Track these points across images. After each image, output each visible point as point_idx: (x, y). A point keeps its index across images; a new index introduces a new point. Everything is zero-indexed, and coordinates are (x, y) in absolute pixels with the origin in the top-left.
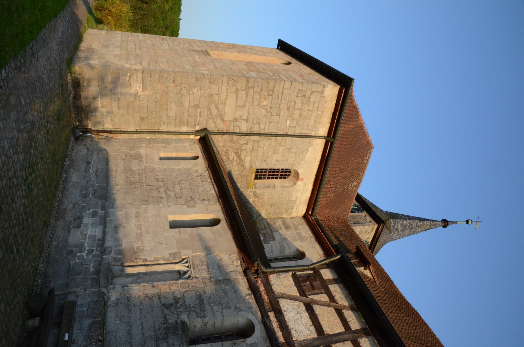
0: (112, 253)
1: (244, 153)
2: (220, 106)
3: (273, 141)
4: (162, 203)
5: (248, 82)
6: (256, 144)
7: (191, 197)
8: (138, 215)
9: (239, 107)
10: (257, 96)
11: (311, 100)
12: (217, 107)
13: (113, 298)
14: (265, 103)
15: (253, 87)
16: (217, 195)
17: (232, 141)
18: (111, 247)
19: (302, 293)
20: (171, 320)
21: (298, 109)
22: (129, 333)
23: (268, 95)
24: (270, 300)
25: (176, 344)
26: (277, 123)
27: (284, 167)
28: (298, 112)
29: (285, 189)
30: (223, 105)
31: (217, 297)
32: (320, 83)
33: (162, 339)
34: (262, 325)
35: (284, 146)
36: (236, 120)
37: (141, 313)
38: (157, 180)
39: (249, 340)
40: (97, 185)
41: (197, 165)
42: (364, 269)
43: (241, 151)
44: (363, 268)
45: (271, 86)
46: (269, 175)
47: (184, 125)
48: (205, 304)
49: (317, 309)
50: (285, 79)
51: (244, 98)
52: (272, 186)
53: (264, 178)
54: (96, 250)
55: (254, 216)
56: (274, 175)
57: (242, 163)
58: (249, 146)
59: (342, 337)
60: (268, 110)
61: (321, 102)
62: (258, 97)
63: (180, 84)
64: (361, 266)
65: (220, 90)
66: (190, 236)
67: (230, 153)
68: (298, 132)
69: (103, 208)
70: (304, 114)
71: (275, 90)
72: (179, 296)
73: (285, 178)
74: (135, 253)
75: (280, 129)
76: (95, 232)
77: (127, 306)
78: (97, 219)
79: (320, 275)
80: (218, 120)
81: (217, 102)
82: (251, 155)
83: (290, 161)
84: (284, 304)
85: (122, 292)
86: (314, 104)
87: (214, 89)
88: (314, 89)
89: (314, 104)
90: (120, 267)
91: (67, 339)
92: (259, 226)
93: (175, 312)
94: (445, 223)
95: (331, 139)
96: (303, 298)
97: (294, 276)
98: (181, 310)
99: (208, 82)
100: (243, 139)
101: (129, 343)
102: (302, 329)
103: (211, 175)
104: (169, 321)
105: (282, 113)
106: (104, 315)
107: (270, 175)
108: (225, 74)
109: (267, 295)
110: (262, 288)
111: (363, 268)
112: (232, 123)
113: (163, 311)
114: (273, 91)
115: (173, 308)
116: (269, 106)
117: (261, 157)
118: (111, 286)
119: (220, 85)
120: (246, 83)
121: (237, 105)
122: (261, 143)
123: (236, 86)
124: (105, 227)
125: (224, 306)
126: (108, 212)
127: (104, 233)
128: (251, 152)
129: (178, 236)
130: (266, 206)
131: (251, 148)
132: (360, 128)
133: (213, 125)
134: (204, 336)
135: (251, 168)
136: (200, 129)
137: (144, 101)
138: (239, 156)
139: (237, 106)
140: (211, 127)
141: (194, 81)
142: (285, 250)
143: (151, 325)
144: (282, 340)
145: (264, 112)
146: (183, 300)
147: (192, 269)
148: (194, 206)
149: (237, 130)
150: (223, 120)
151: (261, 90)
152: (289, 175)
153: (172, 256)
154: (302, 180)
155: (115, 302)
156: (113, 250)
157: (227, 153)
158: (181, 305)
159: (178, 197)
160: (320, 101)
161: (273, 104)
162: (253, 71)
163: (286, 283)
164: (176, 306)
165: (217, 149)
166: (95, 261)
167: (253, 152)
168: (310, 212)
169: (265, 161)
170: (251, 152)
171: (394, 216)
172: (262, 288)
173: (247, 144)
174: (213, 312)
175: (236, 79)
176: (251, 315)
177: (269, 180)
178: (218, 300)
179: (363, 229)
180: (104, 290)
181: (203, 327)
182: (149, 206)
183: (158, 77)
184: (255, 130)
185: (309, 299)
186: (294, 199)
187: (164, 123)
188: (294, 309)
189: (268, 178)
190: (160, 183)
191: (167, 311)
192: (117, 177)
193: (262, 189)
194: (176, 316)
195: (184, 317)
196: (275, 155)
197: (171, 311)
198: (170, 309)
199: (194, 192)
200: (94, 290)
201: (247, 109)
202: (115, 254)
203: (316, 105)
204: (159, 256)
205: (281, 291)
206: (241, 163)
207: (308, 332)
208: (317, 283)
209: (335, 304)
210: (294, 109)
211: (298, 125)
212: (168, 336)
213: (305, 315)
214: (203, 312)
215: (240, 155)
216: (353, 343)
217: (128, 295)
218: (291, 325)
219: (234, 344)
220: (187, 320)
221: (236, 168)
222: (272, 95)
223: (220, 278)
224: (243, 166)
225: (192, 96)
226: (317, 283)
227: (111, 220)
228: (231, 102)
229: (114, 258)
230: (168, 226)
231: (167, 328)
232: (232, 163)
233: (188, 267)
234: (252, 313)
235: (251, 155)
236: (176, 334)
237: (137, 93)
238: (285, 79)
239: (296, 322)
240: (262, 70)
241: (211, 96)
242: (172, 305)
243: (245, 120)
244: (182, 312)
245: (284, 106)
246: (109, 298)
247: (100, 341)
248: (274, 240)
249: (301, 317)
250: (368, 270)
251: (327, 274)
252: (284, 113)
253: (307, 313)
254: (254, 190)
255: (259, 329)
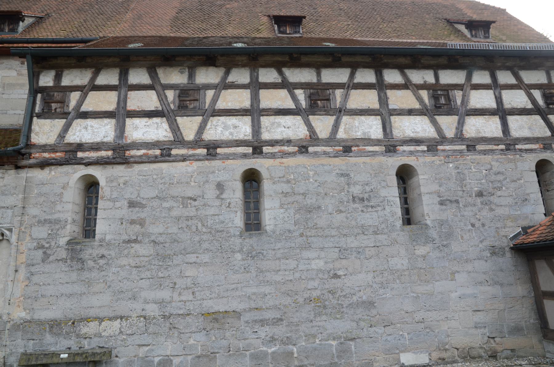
13: (23, 314)
19: (65, 115)
20: (63, 254)
24: (63, 151)
33: (83, 265)
34: (89, 167)
37: (49, 284)
39: (102, 182)
42: (23, 21)
44: (21, 23)
48: (51, 218)
59: (122, 96)
64: (18, 23)
91: (67, 355)
93: (54, 250)
96: (70, 117)
98: (53, 244)
101: (81, 296)
104: (64, 256)
106: (40, 323)
109: (57, 152)
110: (46, 155)
111: (21, 23)
115: (49, 252)
125: (58, 199)
134: (84, 224)
144: (110, 153)
155: (28, 311)
158: (48, 243)
164: (47, 248)
172: (46, 155)
174: (63, 212)
178: (49, 204)
188: (80, 131)
191: (51, 258)
194: (60, 249)
195: (63, 241)
198: (50, 255)
205: (56, 137)
207: (109, 126)
208: (57, 96)
209: (86, 88)
212: (81, 259)
213: (90, 122)
214: (60, 221)
216: (131, 90)
217: (22, 299)
219: (102, 198)
220: (67, 239)
223: (21, 196)
226: (57, 96)
234: (74, 173)
236: (81, 251)
239: (96, 133)
244: (56, 243)
249: (92, 126)
251: (47, 80)
253: (89, 120)
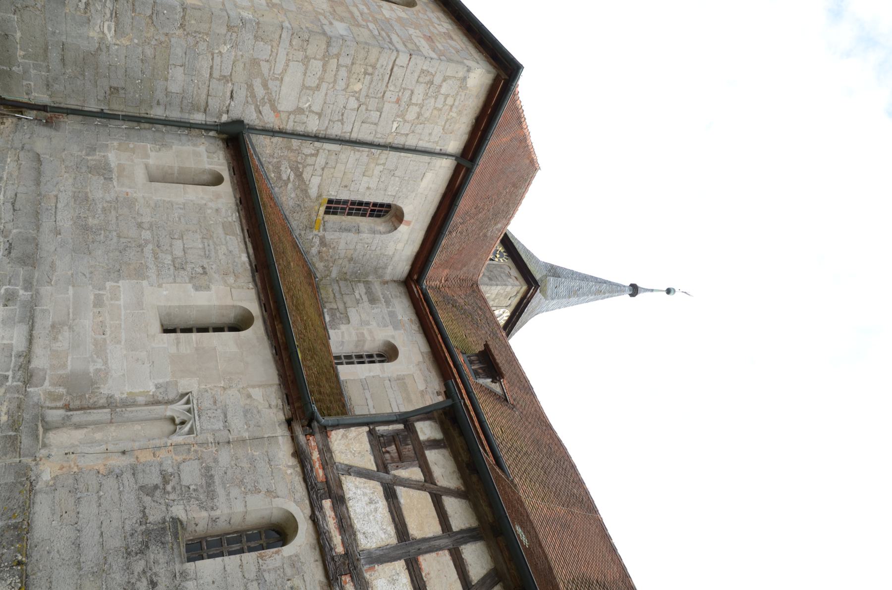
0: (47, 383)
1: (309, 169)
2: (271, 84)
3: (365, 154)
4: (148, 277)
5: (329, 44)
6: (333, 157)
7: (203, 268)
8: (99, 302)
9: (308, 88)
10: (343, 73)
11: (443, 90)
12: (265, 85)
13: (46, 477)
14: (357, 87)
15: (338, 56)
16: (251, 265)
17: (289, 148)
18: (43, 369)
20: (155, 516)
21: (416, 105)
22: (77, 545)
23: (366, 73)
25: (161, 561)
26: (375, 124)
27: (379, 200)
28: (417, 109)
29: (378, 236)
30: (278, 82)
31: (238, 471)
32: (462, 63)
33: (137, 554)
34: (310, 522)
35: (384, 164)
36: (299, 111)
38: (140, 225)
39: (288, 550)
40: (15, 231)
41: (218, 196)
42: (492, 382)
43: (304, 167)
45: (372, 59)
46: (350, 209)
47: (198, 110)
48: (217, 484)
49: (401, 491)
50: (400, 47)
51: (319, 73)
52: (353, 230)
53: (342, 213)
54: (14, 378)
55: (318, 275)
56: (359, 210)
57: (304, 187)
58: (321, 160)
59: (437, 543)
60: (362, 100)
61: (459, 97)
62: (346, 74)
63: (195, 32)
64: (488, 377)
65: (274, 54)
66: (197, 349)
67: (283, 168)
68: (411, 142)
69: (28, 285)
70: (427, 114)
71: (378, 66)
72: (170, 470)
73: (378, 216)
74: (93, 383)
75: (379, 136)
76: (11, 338)
77: (73, 491)
78: (16, 308)
79: (414, 432)
80: (266, 109)
81: (266, 75)
82: (321, 176)
83: (391, 191)
84: (352, 487)
85: (65, 464)
86: (446, 99)
87: (263, 51)
88: (449, 73)
89: (446, 99)
90: (62, 412)
92: (323, 296)
93: (162, 501)
94: (634, 290)
95: (466, 164)
96: (382, 475)
97: (371, 433)
98: (172, 497)
99: (252, 37)
100: (308, 148)
101: (76, 564)
102: (375, 531)
103: (244, 221)
104: (151, 519)
105: (387, 107)
106: (27, 508)
107: (352, 209)
108: (286, 24)
109: (324, 469)
110: (316, 455)
112: (292, 117)
113: (140, 500)
114: (374, 67)
115: (158, 493)
116: (364, 93)
117: (339, 180)
118: (44, 452)
119: (274, 44)
120: (324, 46)
121: (303, 85)
122: (343, 156)
123: (305, 50)
124: (32, 329)
126: (38, 292)
127: (30, 340)
128: (323, 169)
129: (173, 350)
130: (341, 261)
131: (323, 162)
132: (522, 142)
133: (254, 116)
135: (320, 196)
136: (229, 120)
137: (117, 56)
138: (299, 175)
139: (304, 87)
140: (251, 117)
141: (223, 30)
142: (364, 341)
143: (118, 527)
144: (340, 549)
145: (353, 103)
146: (177, 477)
147: (197, 418)
148: (208, 288)
149: (300, 129)
150: (274, 109)
151: (353, 64)
152: (387, 212)
153: (161, 390)
154: (409, 223)
155: (51, 483)
156: (47, 377)
157: (277, 168)
158: (174, 488)
159: (179, 266)
160: (457, 94)
161: (371, 91)
162: (342, 20)
163: (356, 447)
164: (164, 489)
165: (259, 159)
166: (10, 402)
167: (326, 170)
168: (415, 277)
169: (346, 186)
170: (323, 169)
171: (554, 271)
172: (316, 455)
173: (316, 155)
174: (228, 500)
175: (306, 37)
176: (293, 504)
177: (349, 217)
179: (502, 292)
180: (27, 460)
181: (210, 524)
182: (121, 283)
183: (149, 13)
184: (336, 131)
185: (390, 477)
186: (391, 253)
187: (158, 103)
188: (365, 494)
189: (349, 214)
190: (146, 234)
191: (147, 500)
192: (59, 214)
193: (337, 234)
194: (164, 508)
195: (178, 511)
196: (365, 179)
197: (155, 498)
198: (153, 496)
199: (208, 257)
200: (9, 461)
201: (323, 94)
202: (53, 384)
203: (450, 101)
204: (137, 391)
205: (346, 462)
206: (304, 181)
208: (408, 450)
209: (432, 486)
210: (409, 104)
211: (413, 132)
212: (147, 547)
213: (382, 505)
215: (302, 173)
216: (451, 554)
217: (75, 469)
218: (358, 524)
219: (262, 557)
220: (182, 516)
221: (293, 195)
222: (371, 74)
223: (246, 435)
224: (305, 191)
225: (217, 60)
226: (408, 450)
227: (43, 311)
228: (293, 77)
229: (50, 394)
230: (156, 327)
231: (147, 532)
232: (286, 185)
233: (189, 411)
235: (321, 176)
236: (163, 543)
237: (102, 39)
238: (400, 47)
239: (367, 518)
240: (360, 19)
241: (255, 62)
242: (156, 487)
243: (317, 113)
245: (391, 96)
246: (38, 476)
247: (20, 563)
248: (349, 322)
249: (376, 510)
250: (498, 384)
252: (389, 108)
253: (385, 503)
254: (321, 233)
255: (305, 529)
